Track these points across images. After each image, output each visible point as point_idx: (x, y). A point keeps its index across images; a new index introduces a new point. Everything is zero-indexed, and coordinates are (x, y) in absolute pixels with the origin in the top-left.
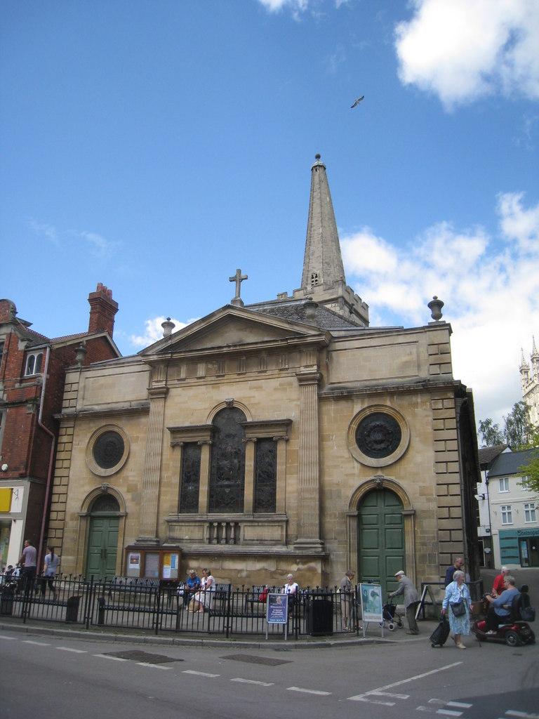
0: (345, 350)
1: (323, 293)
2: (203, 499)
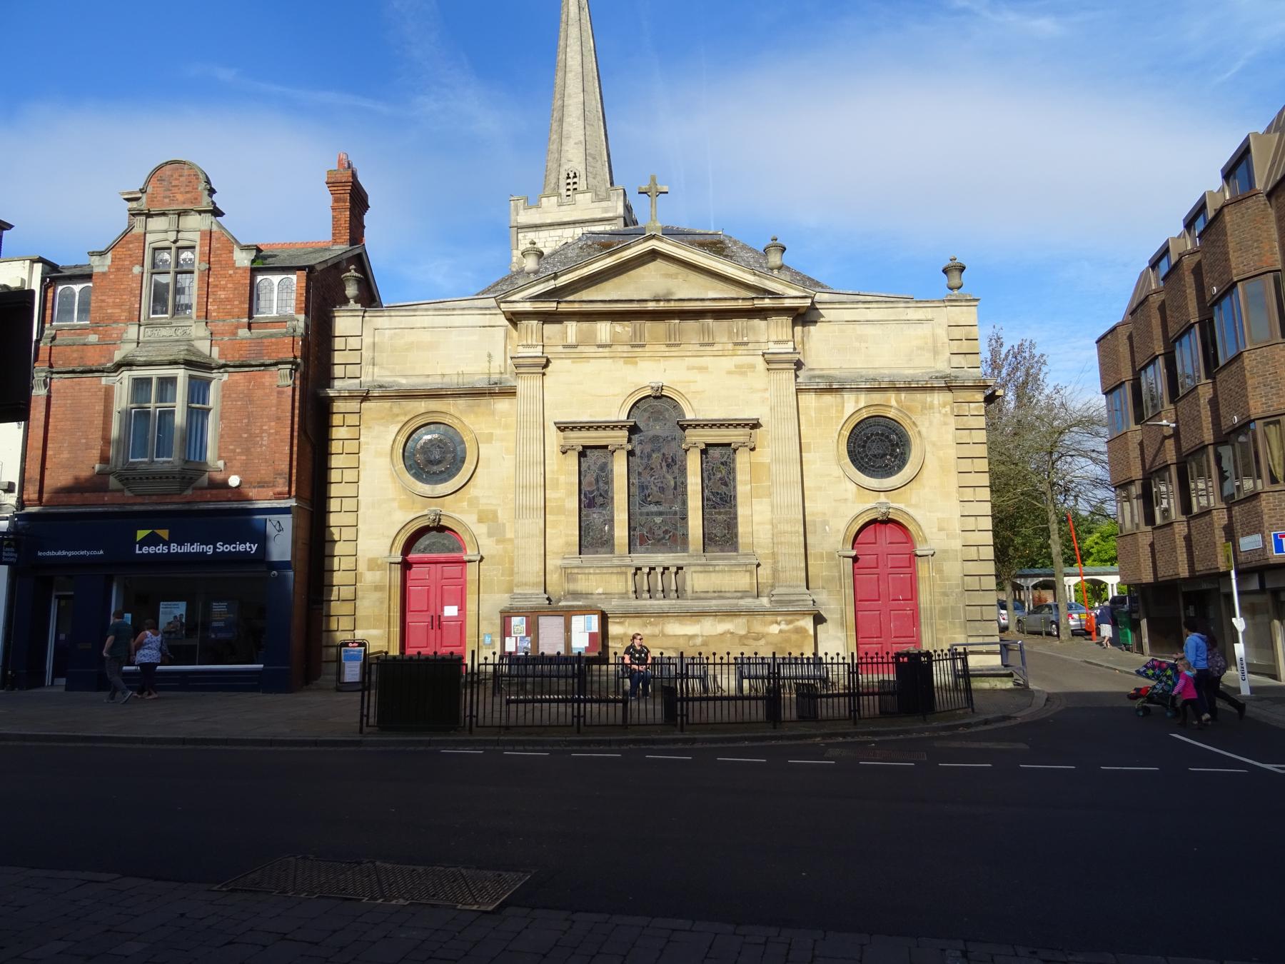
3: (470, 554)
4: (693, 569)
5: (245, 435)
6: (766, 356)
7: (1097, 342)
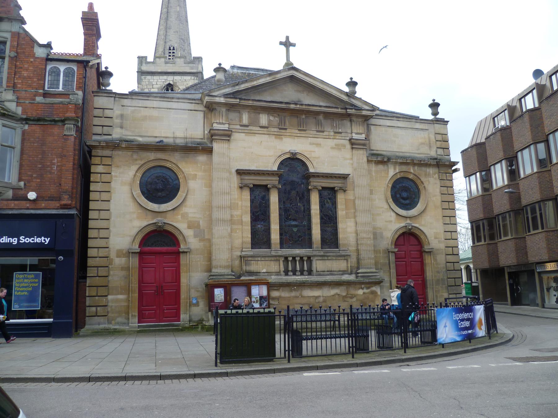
0: (380, 125)
1: (164, 65)
2: (275, 236)
3: (183, 247)
4: (316, 258)
5: (40, 166)
6: (352, 141)
7: (461, 153)
